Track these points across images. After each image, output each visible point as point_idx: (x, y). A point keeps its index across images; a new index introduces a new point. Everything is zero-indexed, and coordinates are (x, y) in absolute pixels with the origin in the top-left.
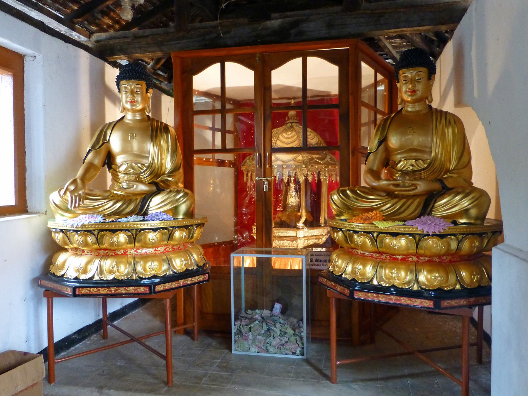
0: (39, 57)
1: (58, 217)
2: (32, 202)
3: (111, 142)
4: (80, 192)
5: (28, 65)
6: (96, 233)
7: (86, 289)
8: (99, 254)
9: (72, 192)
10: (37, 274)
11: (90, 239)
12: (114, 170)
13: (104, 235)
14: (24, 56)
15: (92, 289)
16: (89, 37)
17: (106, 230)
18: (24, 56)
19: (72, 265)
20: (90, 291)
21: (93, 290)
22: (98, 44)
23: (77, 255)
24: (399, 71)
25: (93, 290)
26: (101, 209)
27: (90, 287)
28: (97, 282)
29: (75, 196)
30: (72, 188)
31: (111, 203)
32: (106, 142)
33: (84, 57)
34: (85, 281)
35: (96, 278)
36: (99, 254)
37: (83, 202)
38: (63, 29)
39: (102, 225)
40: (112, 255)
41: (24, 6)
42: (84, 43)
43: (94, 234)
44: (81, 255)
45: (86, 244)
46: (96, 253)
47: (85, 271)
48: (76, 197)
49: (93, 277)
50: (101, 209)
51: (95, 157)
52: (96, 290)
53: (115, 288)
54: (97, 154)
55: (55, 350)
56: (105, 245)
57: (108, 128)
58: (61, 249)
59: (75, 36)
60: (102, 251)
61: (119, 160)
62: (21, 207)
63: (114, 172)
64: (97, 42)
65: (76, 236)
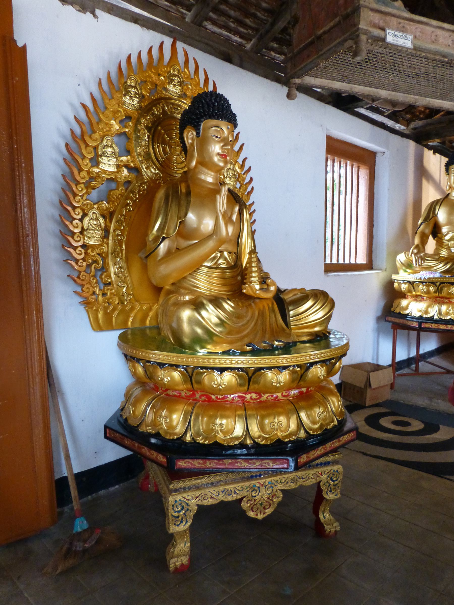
0: (387, 153)
1: (401, 272)
2: (376, 263)
3: (439, 215)
4: (422, 254)
5: (379, 159)
6: (438, 284)
7: (423, 326)
8: (436, 300)
9: (415, 254)
10: (379, 314)
11: (432, 289)
12: (439, 238)
13: (444, 286)
14: (376, 153)
15: (433, 325)
16: (407, 126)
17: (447, 283)
18: (376, 153)
19: (414, 308)
20: (432, 326)
21: (434, 326)
22: (415, 131)
23: (416, 301)
24: (342, 465)
25: (434, 326)
26: (435, 268)
27: (432, 323)
28: (436, 320)
29: (418, 257)
30: (415, 251)
31: (441, 265)
32: (435, 216)
33: (412, 144)
34: (426, 319)
35: (436, 317)
36: (436, 300)
37: (424, 262)
38: (390, 123)
39: (443, 279)
40: (447, 302)
41: (370, 113)
42: (402, 131)
43: (436, 285)
44: (420, 301)
45: (428, 292)
46: (434, 300)
47: (426, 312)
48: (418, 258)
49: (433, 316)
50: (435, 268)
51: (425, 228)
52: (436, 325)
53: (451, 326)
54: (427, 225)
55: (397, 366)
56: (444, 294)
57: (436, 205)
58: (403, 295)
59: (398, 127)
60: (438, 299)
61: (444, 230)
62: (369, 266)
63: (439, 240)
64: (414, 129)
65: (421, 286)
